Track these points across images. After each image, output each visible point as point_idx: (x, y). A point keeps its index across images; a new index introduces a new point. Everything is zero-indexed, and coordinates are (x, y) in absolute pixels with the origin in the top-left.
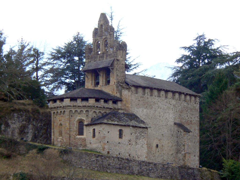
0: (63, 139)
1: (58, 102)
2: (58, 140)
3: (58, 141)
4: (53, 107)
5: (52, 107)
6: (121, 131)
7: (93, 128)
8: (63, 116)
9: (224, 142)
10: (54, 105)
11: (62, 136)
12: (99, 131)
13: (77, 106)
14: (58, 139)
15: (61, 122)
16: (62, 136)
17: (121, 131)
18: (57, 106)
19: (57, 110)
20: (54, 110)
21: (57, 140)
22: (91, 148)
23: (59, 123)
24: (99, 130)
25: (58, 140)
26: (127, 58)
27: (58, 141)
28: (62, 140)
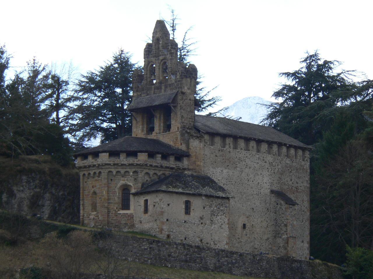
0: (98, 216)
2: (90, 216)
3: (90, 219)
6: (188, 204)
7: (145, 199)
8: (99, 180)
10: (83, 163)
12: (154, 203)
13: (120, 164)
14: (90, 215)
17: (188, 204)
20: (85, 170)
21: (89, 217)
23: (92, 191)
24: (155, 201)
27: (90, 218)
28: (96, 217)
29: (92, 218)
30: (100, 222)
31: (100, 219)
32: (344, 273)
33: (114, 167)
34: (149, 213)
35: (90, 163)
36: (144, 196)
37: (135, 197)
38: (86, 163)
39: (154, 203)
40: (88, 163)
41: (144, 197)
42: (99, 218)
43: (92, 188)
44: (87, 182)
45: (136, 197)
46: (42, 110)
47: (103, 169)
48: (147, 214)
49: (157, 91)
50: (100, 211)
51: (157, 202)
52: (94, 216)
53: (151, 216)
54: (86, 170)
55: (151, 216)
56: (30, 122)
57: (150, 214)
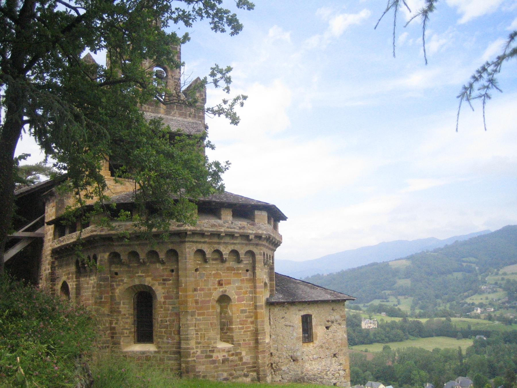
0: (240, 353)
1: (227, 216)
2: (215, 355)
3: (214, 362)
4: (208, 231)
5: (205, 229)
6: (306, 321)
7: (303, 313)
8: (238, 269)
9: (240, 343)
10: (213, 226)
11: (232, 344)
12: (328, 321)
13: (224, 234)
14: (213, 351)
15: (225, 288)
16: (228, 339)
17: (306, 321)
18: (230, 230)
19: (219, 243)
20: (204, 242)
21: (211, 357)
22: (299, 373)
23: (216, 295)
24: (329, 318)
25: (215, 355)
26: (16, 155)
27: (214, 358)
28: (233, 355)
29: (221, 358)
30: (245, 366)
31: (244, 360)
32: (245, 378)
33: (138, 243)
34: (317, 342)
35: (234, 228)
36: (301, 309)
37: (272, 310)
38: (220, 226)
39: (328, 321)
40: (228, 228)
41: (300, 310)
42: (241, 359)
43: (216, 287)
44: (200, 270)
45: (279, 308)
46: (58, 12)
47: (259, 247)
48: (311, 344)
49: (147, 107)
50: (244, 340)
51: (337, 321)
52: (226, 354)
53: (322, 347)
54: (209, 243)
55: (322, 347)
56: (37, 28)
57: (321, 344)
